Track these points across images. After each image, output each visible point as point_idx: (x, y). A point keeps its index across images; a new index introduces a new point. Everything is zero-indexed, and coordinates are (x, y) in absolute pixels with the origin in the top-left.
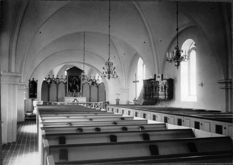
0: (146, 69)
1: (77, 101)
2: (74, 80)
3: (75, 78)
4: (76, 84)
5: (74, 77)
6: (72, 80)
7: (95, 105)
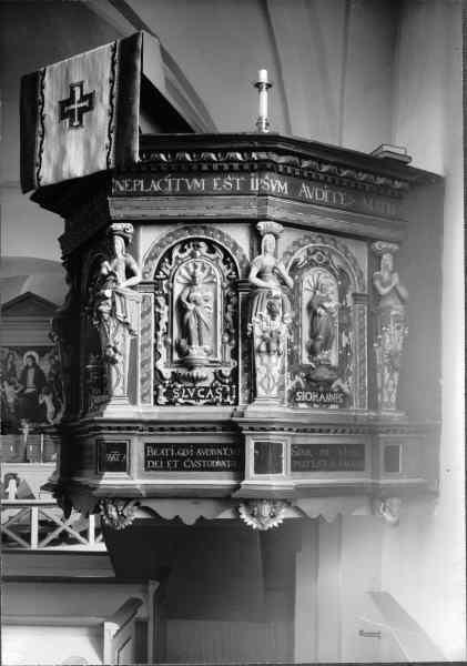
0: (438, 416)
1: (18, 485)
2: (27, 368)
3: (34, 354)
4: (39, 392)
5: (29, 353)
6: (19, 370)
7: (55, 535)
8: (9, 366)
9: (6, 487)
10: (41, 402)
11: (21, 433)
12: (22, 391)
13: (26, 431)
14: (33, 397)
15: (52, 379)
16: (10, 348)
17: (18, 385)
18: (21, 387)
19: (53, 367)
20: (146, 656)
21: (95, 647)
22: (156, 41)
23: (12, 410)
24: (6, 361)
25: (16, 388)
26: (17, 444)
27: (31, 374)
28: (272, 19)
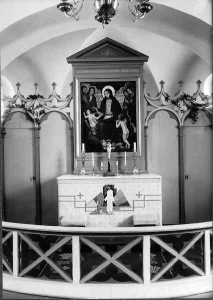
2: (106, 99)
5: (106, 87)
6: (99, 100)
8: (91, 98)
9: (105, 197)
10: (117, 126)
11: (106, 151)
12: (103, 117)
13: (109, 149)
14: (112, 121)
15: (126, 108)
16: (91, 84)
17: (98, 112)
18: (101, 115)
19: (126, 98)
20: (189, 259)
21: (60, 281)
22: (175, 121)
23: (94, 133)
24: (88, 93)
25: (97, 116)
26: (99, 160)
27: (109, 104)
28: (177, 175)
